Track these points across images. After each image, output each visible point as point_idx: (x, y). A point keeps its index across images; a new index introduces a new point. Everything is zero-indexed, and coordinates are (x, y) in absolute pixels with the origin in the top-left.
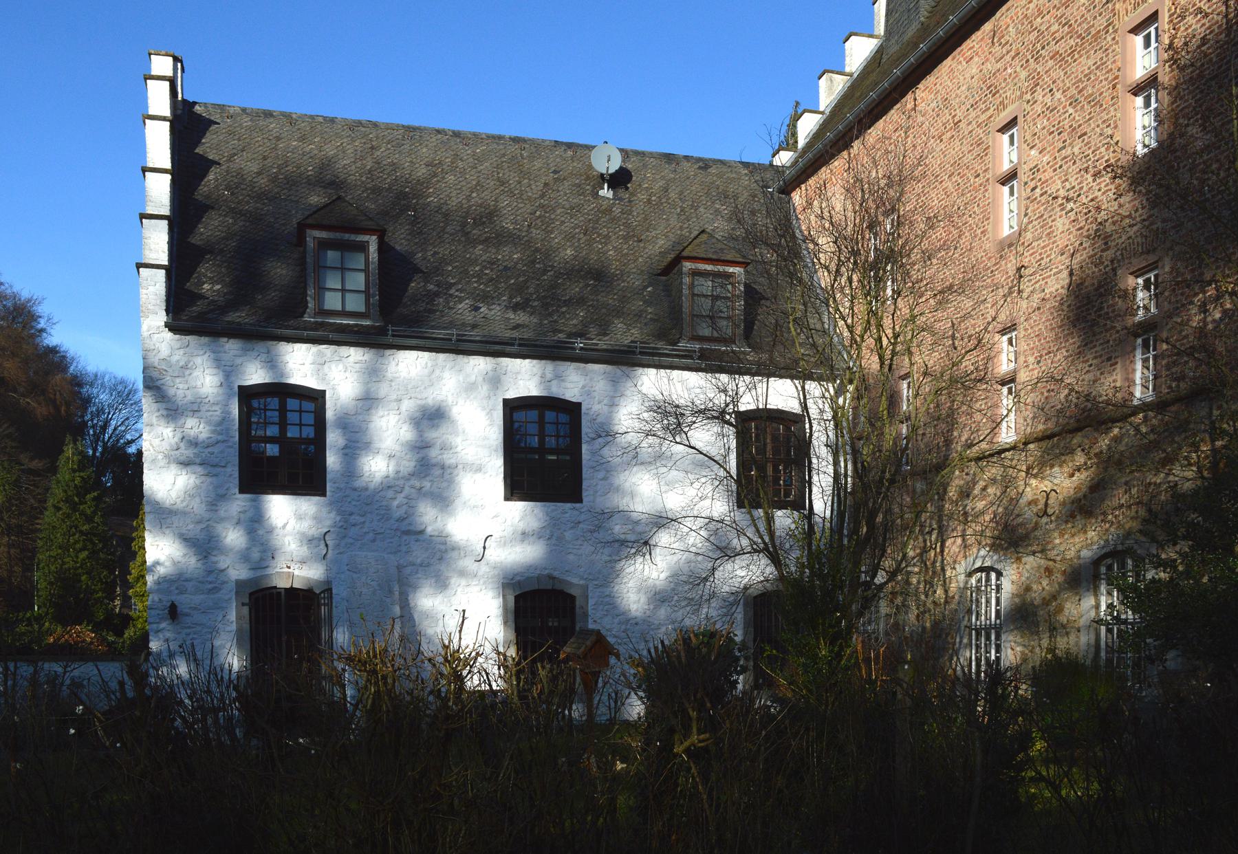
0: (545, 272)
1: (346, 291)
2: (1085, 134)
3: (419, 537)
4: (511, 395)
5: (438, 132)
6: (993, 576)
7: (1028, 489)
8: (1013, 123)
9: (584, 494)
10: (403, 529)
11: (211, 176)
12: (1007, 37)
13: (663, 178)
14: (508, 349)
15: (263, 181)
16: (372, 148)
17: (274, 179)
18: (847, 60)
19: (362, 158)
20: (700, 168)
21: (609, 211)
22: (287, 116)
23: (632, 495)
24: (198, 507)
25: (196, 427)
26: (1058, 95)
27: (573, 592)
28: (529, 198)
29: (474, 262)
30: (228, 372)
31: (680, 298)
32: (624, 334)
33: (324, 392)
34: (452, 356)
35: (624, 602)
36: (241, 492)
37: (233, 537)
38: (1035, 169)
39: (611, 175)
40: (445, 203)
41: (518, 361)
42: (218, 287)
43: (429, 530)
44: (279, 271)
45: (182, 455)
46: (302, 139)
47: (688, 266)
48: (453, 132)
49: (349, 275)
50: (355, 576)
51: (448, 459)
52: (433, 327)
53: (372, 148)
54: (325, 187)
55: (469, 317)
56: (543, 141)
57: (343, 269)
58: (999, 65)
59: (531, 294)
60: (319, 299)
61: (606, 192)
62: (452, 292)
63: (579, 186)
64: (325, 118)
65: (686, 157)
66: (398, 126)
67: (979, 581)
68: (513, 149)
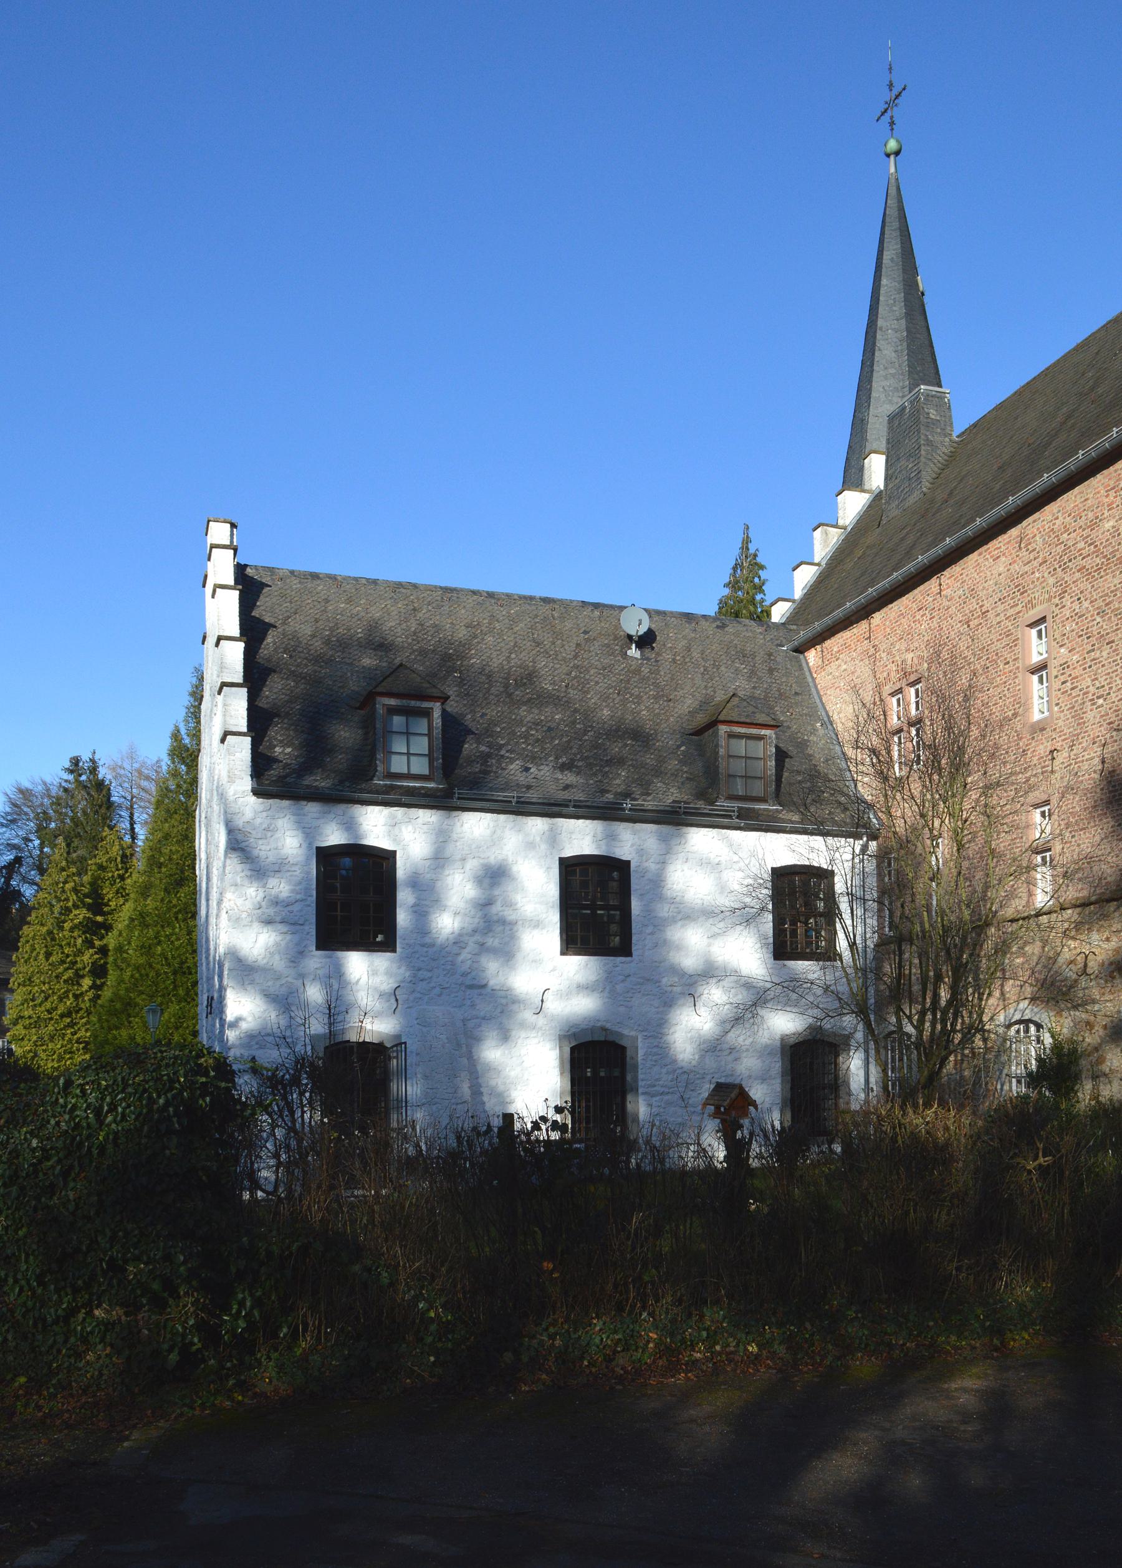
0: (585, 732)
1: (409, 755)
2: (1113, 642)
3: (483, 991)
4: (568, 853)
5: (474, 592)
6: (1033, 1028)
7: (1066, 949)
8: (1043, 620)
9: (634, 948)
10: (468, 982)
11: (269, 639)
12: (1034, 545)
13: (684, 637)
14: (565, 810)
15: (317, 644)
16: (414, 609)
17: (328, 642)
18: (840, 513)
19: (406, 620)
20: (718, 627)
21: (637, 671)
22: (333, 578)
23: (679, 948)
24: (279, 964)
25: (281, 887)
26: (1086, 604)
27: (624, 1043)
28: (564, 659)
29: (520, 723)
30: (309, 833)
31: (716, 759)
32: (670, 794)
33: (395, 852)
34: (511, 817)
35: (671, 1052)
36: (318, 948)
37: (314, 994)
38: (1065, 666)
39: (640, 637)
40: (487, 665)
41: (572, 820)
42: (289, 750)
43: (492, 983)
44: (345, 734)
45: (263, 914)
46: (349, 601)
47: (723, 729)
48: (487, 593)
49: (413, 739)
50: (425, 1030)
51: (511, 916)
52: (491, 789)
53: (414, 609)
54: (375, 649)
55: (522, 778)
56: (571, 601)
57: (408, 734)
58: (1026, 568)
59: (575, 755)
60: (387, 762)
61: (633, 652)
62: (502, 752)
63: (608, 646)
64: (367, 579)
65: (704, 616)
66: (436, 587)
67: (1018, 1032)
68: (545, 610)
